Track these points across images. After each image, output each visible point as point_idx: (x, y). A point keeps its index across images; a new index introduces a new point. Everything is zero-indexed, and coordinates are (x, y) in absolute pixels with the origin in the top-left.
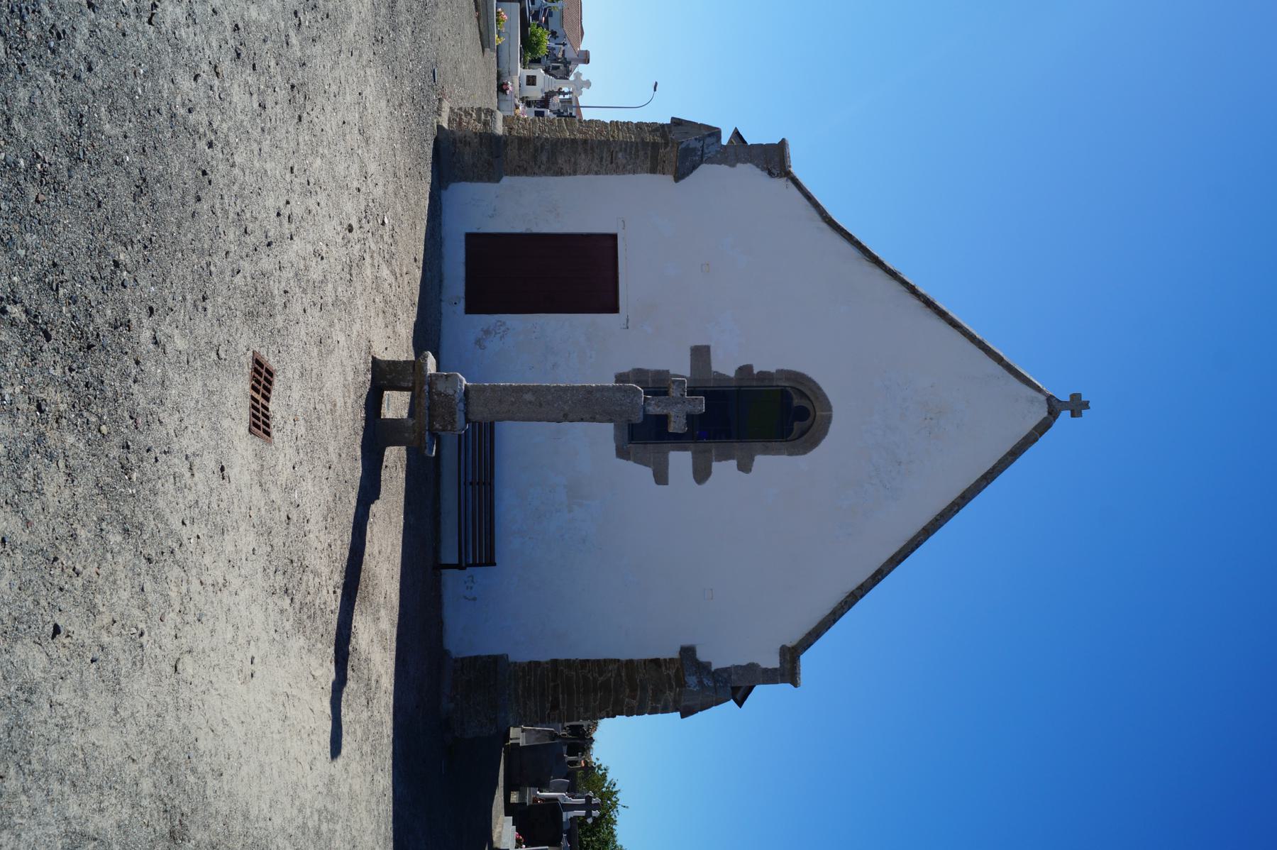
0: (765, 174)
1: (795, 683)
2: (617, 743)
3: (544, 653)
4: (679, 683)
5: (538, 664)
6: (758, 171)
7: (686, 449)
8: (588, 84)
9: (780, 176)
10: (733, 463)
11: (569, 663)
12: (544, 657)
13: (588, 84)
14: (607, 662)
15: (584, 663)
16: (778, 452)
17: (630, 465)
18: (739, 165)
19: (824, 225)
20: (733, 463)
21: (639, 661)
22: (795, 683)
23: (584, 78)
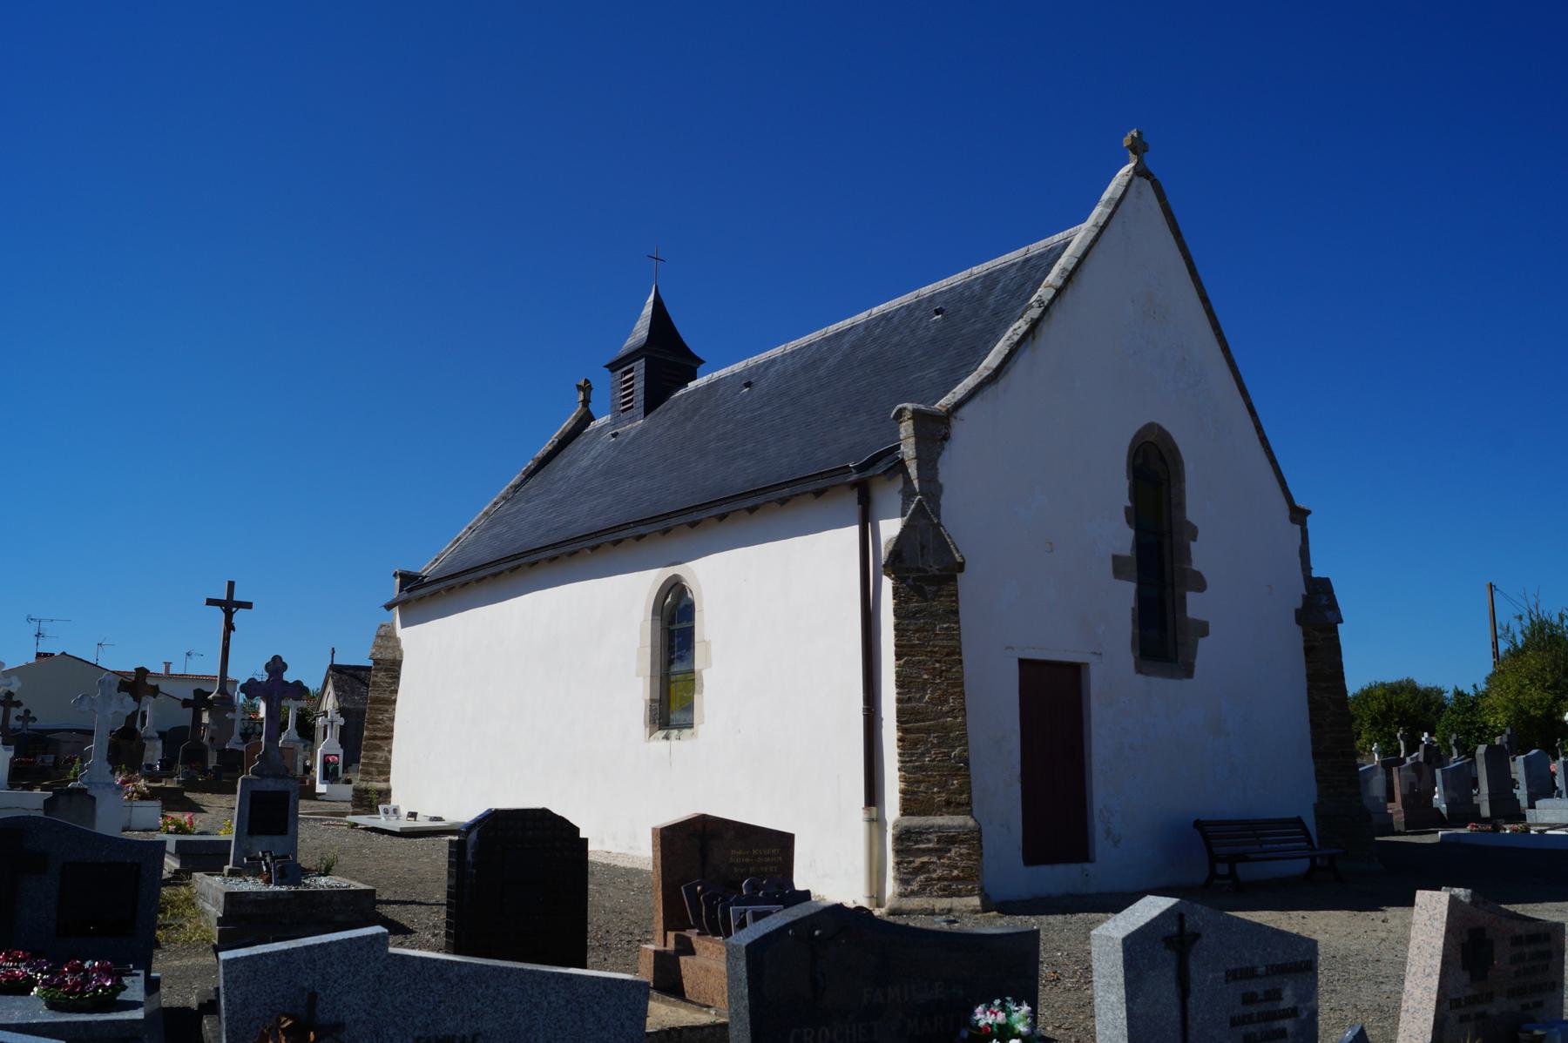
0: (947, 445)
1: (1309, 512)
2: (1356, 680)
3: (1313, 786)
4: (1318, 613)
5: (1318, 772)
6: (945, 455)
7: (1184, 598)
8: (276, 666)
9: (948, 426)
10: (1192, 544)
11: (1316, 739)
12: (1310, 767)
13: (276, 666)
14: (1311, 701)
15: (1315, 725)
16: (1182, 492)
17: (1199, 662)
18: (941, 480)
19: (1002, 382)
20: (1192, 544)
21: (1308, 668)
22: (1309, 512)
23: (262, 676)
